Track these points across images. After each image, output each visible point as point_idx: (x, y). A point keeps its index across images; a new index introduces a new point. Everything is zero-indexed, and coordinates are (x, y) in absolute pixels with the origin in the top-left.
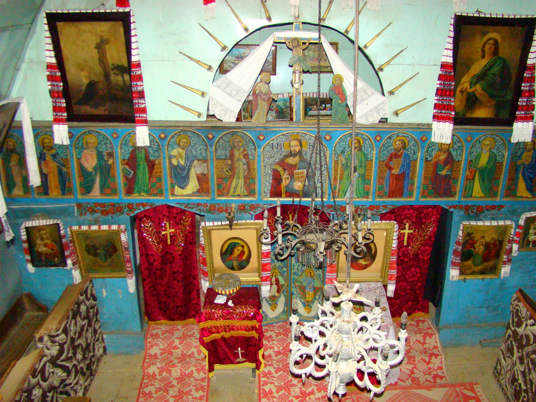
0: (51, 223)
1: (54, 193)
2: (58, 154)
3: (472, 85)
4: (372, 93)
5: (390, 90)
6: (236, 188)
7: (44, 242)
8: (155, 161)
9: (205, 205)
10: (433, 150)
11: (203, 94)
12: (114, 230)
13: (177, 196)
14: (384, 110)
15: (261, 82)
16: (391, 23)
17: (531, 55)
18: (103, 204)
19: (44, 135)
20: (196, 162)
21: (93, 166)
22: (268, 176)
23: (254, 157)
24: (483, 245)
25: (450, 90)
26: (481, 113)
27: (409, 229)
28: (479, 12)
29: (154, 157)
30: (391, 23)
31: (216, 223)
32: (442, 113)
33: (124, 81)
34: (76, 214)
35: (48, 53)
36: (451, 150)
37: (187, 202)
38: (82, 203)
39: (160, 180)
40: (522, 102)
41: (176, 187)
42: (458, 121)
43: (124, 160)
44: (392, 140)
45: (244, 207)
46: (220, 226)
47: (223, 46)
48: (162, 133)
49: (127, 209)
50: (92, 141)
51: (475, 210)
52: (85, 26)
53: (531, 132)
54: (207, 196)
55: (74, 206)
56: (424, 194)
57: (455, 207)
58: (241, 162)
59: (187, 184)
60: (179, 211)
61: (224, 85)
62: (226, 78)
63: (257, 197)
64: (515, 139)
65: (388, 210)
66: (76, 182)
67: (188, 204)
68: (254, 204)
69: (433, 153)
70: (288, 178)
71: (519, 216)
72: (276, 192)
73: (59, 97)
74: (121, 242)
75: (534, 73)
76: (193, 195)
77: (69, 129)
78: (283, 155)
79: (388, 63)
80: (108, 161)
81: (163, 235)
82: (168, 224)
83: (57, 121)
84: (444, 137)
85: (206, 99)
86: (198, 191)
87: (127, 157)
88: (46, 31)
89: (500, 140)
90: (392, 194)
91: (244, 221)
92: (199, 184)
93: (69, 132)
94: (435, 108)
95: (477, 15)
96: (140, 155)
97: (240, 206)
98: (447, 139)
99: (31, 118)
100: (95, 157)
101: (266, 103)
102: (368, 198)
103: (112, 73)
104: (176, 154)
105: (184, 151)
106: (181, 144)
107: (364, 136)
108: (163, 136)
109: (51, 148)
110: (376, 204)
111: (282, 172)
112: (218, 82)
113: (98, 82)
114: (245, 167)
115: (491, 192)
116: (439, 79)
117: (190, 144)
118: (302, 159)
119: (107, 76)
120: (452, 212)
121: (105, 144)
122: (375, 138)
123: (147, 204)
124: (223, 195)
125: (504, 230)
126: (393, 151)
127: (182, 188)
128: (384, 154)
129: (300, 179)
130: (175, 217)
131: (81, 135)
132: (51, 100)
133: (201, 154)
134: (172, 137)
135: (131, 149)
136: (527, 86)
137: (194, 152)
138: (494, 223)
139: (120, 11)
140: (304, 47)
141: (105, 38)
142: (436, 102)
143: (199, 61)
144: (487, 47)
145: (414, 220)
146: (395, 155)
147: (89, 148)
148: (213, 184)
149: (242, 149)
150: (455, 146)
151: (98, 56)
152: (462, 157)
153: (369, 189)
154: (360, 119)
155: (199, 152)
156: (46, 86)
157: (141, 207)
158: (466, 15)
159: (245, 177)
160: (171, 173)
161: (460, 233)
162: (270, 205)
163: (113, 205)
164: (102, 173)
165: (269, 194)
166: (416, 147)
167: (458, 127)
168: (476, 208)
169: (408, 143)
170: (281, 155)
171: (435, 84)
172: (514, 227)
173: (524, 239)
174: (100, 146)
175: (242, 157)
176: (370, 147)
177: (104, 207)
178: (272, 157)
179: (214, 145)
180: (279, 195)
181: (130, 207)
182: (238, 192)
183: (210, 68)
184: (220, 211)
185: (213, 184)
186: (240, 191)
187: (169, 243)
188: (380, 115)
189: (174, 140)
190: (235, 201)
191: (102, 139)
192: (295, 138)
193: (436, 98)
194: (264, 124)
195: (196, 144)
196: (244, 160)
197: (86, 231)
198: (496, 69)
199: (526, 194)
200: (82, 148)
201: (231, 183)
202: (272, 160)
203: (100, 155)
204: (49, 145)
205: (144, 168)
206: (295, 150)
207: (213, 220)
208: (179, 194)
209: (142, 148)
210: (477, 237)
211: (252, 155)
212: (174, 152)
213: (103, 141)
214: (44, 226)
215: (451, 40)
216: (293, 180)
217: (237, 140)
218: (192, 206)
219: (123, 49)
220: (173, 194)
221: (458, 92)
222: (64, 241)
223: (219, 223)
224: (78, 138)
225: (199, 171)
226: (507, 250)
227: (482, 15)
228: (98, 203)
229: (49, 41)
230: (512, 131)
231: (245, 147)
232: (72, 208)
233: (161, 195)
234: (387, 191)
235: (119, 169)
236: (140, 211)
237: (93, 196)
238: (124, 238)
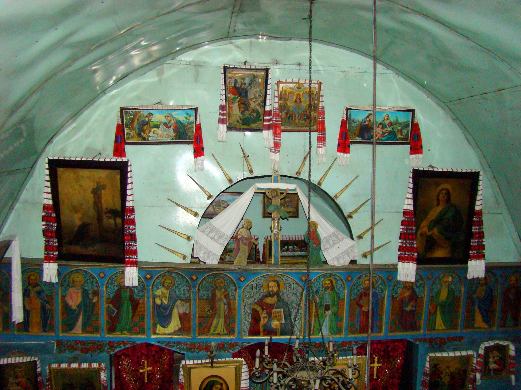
0: (28, 360)
1: (35, 330)
2: (43, 291)
3: (430, 229)
4: (343, 238)
5: (358, 234)
6: (216, 328)
7: (17, 381)
8: (139, 301)
9: (185, 344)
10: (398, 288)
11: (189, 238)
12: (94, 368)
13: (159, 334)
14: (354, 252)
15: (243, 228)
16: (357, 176)
17: (477, 203)
18: (82, 341)
19: (31, 272)
20: (179, 302)
21: (77, 304)
22: (247, 315)
23: (235, 297)
24: (448, 375)
25: (412, 234)
26: (440, 253)
27: (378, 362)
28: (432, 167)
29: (139, 296)
30: (357, 176)
31: (196, 362)
32: (405, 254)
33: (116, 223)
34: (55, 352)
35: (46, 195)
36: (415, 287)
37: (168, 340)
38: (62, 340)
39: (143, 319)
40: (474, 242)
41: (158, 326)
42: (419, 261)
43: (108, 298)
44: (361, 280)
45: (223, 345)
46: (200, 364)
47: (208, 195)
48: (148, 274)
49: (108, 347)
50: (78, 279)
51: (438, 342)
52: (85, 173)
53: (484, 269)
54: (188, 334)
55: (53, 343)
56: (392, 329)
57: (420, 340)
58: (221, 302)
59: (170, 322)
60: (158, 349)
61: (208, 231)
62: (211, 224)
63: (236, 336)
64: (470, 275)
65: (359, 345)
66: (59, 320)
67: (169, 343)
68: (233, 342)
69: (398, 290)
70: (266, 317)
71: (478, 346)
72: (254, 331)
73: (51, 237)
74: (100, 381)
75: (482, 217)
76: (175, 333)
77: (58, 268)
78: (261, 295)
79: (356, 211)
80: (93, 299)
81: (141, 373)
82: (146, 362)
83: (48, 259)
84: (409, 275)
85: (192, 243)
86: (180, 330)
87: (112, 295)
88: (46, 175)
89: (457, 277)
90: (364, 329)
91: (224, 359)
92: (181, 324)
93: (58, 270)
94: (399, 250)
95: (431, 169)
96: (125, 294)
97: (219, 345)
98: (412, 278)
99: (21, 255)
100: (80, 295)
101: (247, 247)
102: (341, 335)
103: (105, 216)
104: (160, 294)
105: (168, 291)
106: (166, 285)
107: (337, 277)
108: (148, 276)
109: (37, 285)
110: (349, 340)
111: (260, 312)
112: (203, 227)
113: (91, 224)
114: (226, 306)
115: (451, 324)
116: (402, 225)
117: (174, 284)
118: (280, 299)
119: (99, 219)
120: (418, 345)
121: (92, 282)
122: (347, 279)
123: (128, 343)
124: (203, 334)
125: (467, 359)
126: (362, 290)
127: (164, 327)
128: (354, 293)
129: (278, 318)
130: (154, 356)
131: (68, 273)
132: (44, 239)
133: (184, 294)
134: (158, 278)
135: (116, 288)
136: (477, 229)
137: (177, 292)
138: (458, 354)
139: (118, 160)
140: (282, 196)
141: (102, 184)
142: (400, 244)
143: (186, 208)
144: (441, 196)
145: (382, 353)
146: (365, 294)
147: (75, 287)
148: (194, 323)
149: (223, 290)
150: (418, 284)
151: (93, 200)
152: (425, 295)
153: (341, 326)
154: (332, 261)
155: (183, 292)
156: (41, 225)
157: (122, 345)
158: (422, 169)
159: (225, 317)
160: (154, 312)
161: (427, 365)
162: (249, 343)
163: (93, 343)
164: (85, 312)
165: (248, 332)
166: (383, 285)
167: (421, 266)
168: (439, 340)
169: (376, 283)
170: (259, 295)
171: (399, 229)
172: (475, 356)
173: (485, 368)
174: (86, 285)
175: (223, 297)
176: (342, 286)
177: (85, 344)
178: (251, 297)
179: (198, 285)
180: (258, 333)
181: (111, 345)
182: (218, 331)
183: (196, 214)
184: (200, 349)
185: (194, 323)
186: (220, 330)
187: (146, 381)
188: (350, 258)
189: (159, 281)
190: (214, 340)
191: (88, 278)
192: (273, 279)
193: (400, 241)
194: (245, 266)
195: (180, 284)
196: (225, 300)
197: (65, 369)
198: (449, 215)
199: (483, 325)
200: (68, 286)
201: (213, 320)
202: (251, 300)
203: (85, 293)
204: (35, 282)
205: (128, 307)
206: (272, 291)
207: (193, 359)
208: (160, 332)
209: (128, 287)
210: (442, 367)
211: (232, 295)
212: (158, 292)
213: (90, 279)
214: (19, 363)
215: (411, 191)
216: (270, 319)
217: (219, 281)
218: (173, 344)
219: (118, 194)
220: (155, 333)
221: (418, 235)
222: (39, 379)
223: (200, 362)
224: (65, 276)
225: (182, 310)
226: (471, 379)
227: (435, 170)
228: (79, 341)
229: (48, 184)
230: (467, 269)
231: (227, 288)
232: (52, 345)
233: (143, 333)
234: (358, 327)
235: (103, 307)
236: (120, 349)
237: (75, 333)
238: (103, 376)
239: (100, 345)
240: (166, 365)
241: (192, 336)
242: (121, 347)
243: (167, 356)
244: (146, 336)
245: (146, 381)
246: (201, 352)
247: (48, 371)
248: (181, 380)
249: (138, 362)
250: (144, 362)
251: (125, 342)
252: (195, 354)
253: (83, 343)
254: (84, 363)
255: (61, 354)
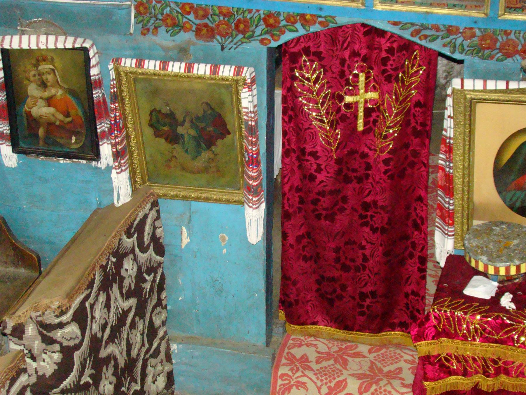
0: (69, 46)
7: (46, 94)
18: (200, 7)
31: (491, 85)
37: (418, 21)
49: (262, 27)
81: (348, 106)
82: (362, 78)
130: (385, 61)
157: (298, 25)
177: (205, 16)
187: (360, 127)
218: (433, 32)
223: (501, 85)
228: (191, 6)
232: (123, 12)
239: (246, 22)
240: (415, 88)
241: (488, 11)
242: (297, 31)
243: (419, 65)
244: (363, 4)
245: (360, 127)
246: (510, 60)
247: (113, 75)
248: (446, 131)
249: (342, 74)
250: (356, 76)
251: (308, 17)
252: (491, 64)
253: (201, 13)
254: (199, 62)
255: (150, 37)
